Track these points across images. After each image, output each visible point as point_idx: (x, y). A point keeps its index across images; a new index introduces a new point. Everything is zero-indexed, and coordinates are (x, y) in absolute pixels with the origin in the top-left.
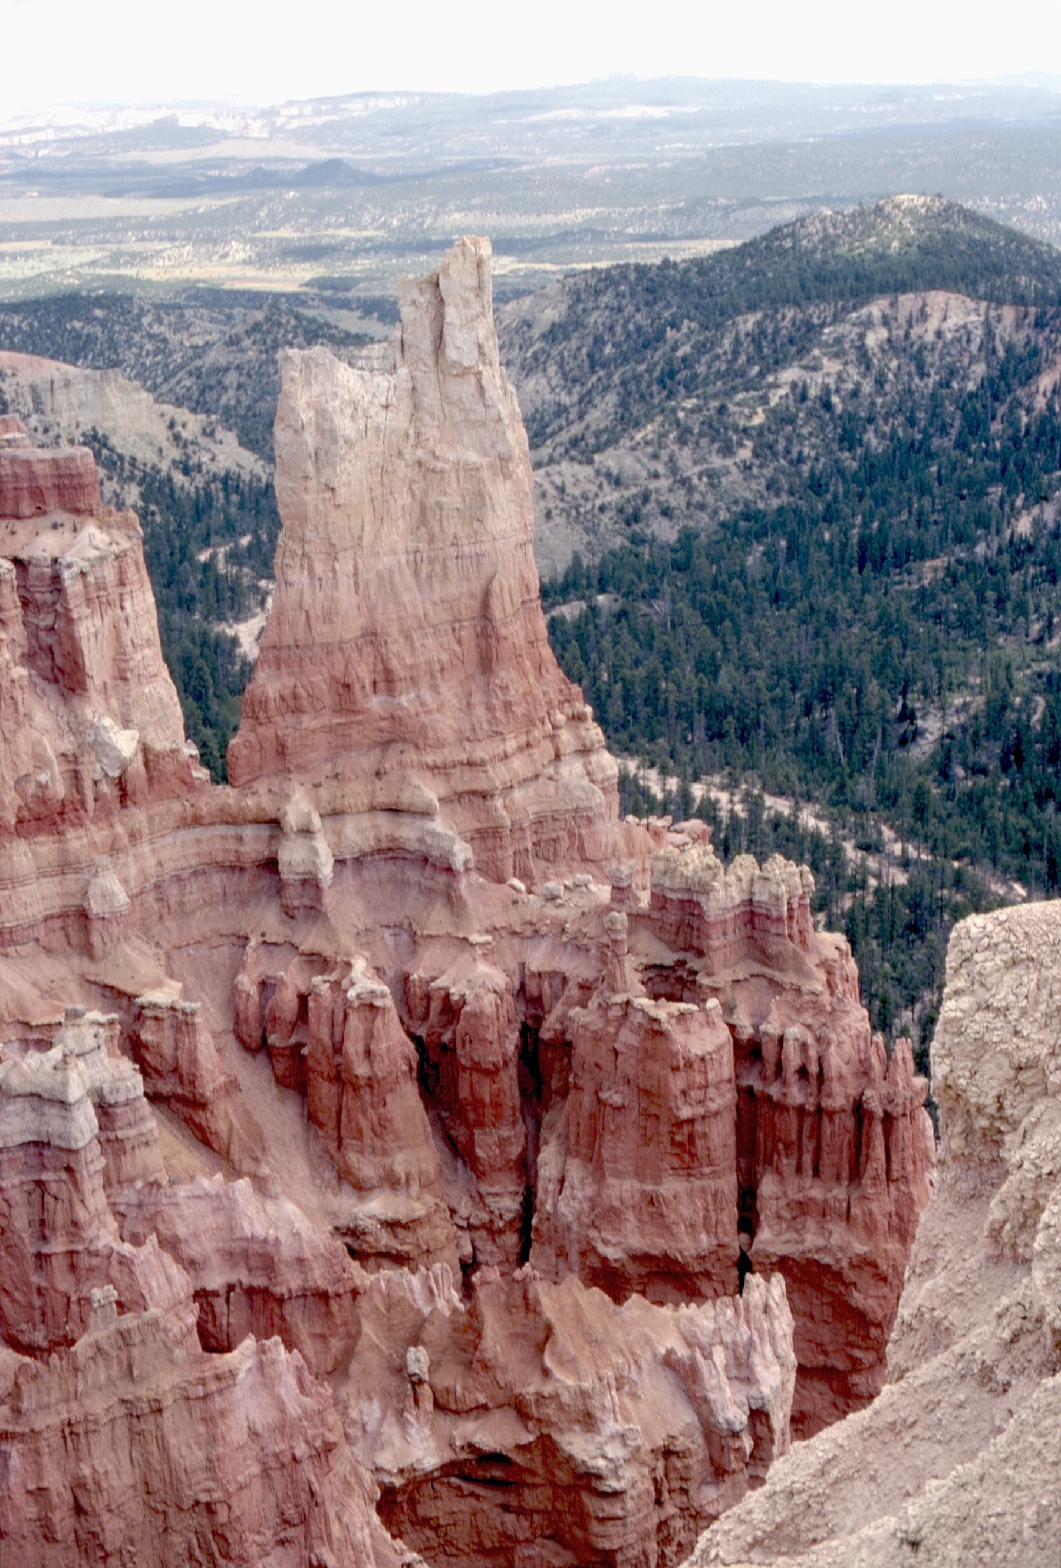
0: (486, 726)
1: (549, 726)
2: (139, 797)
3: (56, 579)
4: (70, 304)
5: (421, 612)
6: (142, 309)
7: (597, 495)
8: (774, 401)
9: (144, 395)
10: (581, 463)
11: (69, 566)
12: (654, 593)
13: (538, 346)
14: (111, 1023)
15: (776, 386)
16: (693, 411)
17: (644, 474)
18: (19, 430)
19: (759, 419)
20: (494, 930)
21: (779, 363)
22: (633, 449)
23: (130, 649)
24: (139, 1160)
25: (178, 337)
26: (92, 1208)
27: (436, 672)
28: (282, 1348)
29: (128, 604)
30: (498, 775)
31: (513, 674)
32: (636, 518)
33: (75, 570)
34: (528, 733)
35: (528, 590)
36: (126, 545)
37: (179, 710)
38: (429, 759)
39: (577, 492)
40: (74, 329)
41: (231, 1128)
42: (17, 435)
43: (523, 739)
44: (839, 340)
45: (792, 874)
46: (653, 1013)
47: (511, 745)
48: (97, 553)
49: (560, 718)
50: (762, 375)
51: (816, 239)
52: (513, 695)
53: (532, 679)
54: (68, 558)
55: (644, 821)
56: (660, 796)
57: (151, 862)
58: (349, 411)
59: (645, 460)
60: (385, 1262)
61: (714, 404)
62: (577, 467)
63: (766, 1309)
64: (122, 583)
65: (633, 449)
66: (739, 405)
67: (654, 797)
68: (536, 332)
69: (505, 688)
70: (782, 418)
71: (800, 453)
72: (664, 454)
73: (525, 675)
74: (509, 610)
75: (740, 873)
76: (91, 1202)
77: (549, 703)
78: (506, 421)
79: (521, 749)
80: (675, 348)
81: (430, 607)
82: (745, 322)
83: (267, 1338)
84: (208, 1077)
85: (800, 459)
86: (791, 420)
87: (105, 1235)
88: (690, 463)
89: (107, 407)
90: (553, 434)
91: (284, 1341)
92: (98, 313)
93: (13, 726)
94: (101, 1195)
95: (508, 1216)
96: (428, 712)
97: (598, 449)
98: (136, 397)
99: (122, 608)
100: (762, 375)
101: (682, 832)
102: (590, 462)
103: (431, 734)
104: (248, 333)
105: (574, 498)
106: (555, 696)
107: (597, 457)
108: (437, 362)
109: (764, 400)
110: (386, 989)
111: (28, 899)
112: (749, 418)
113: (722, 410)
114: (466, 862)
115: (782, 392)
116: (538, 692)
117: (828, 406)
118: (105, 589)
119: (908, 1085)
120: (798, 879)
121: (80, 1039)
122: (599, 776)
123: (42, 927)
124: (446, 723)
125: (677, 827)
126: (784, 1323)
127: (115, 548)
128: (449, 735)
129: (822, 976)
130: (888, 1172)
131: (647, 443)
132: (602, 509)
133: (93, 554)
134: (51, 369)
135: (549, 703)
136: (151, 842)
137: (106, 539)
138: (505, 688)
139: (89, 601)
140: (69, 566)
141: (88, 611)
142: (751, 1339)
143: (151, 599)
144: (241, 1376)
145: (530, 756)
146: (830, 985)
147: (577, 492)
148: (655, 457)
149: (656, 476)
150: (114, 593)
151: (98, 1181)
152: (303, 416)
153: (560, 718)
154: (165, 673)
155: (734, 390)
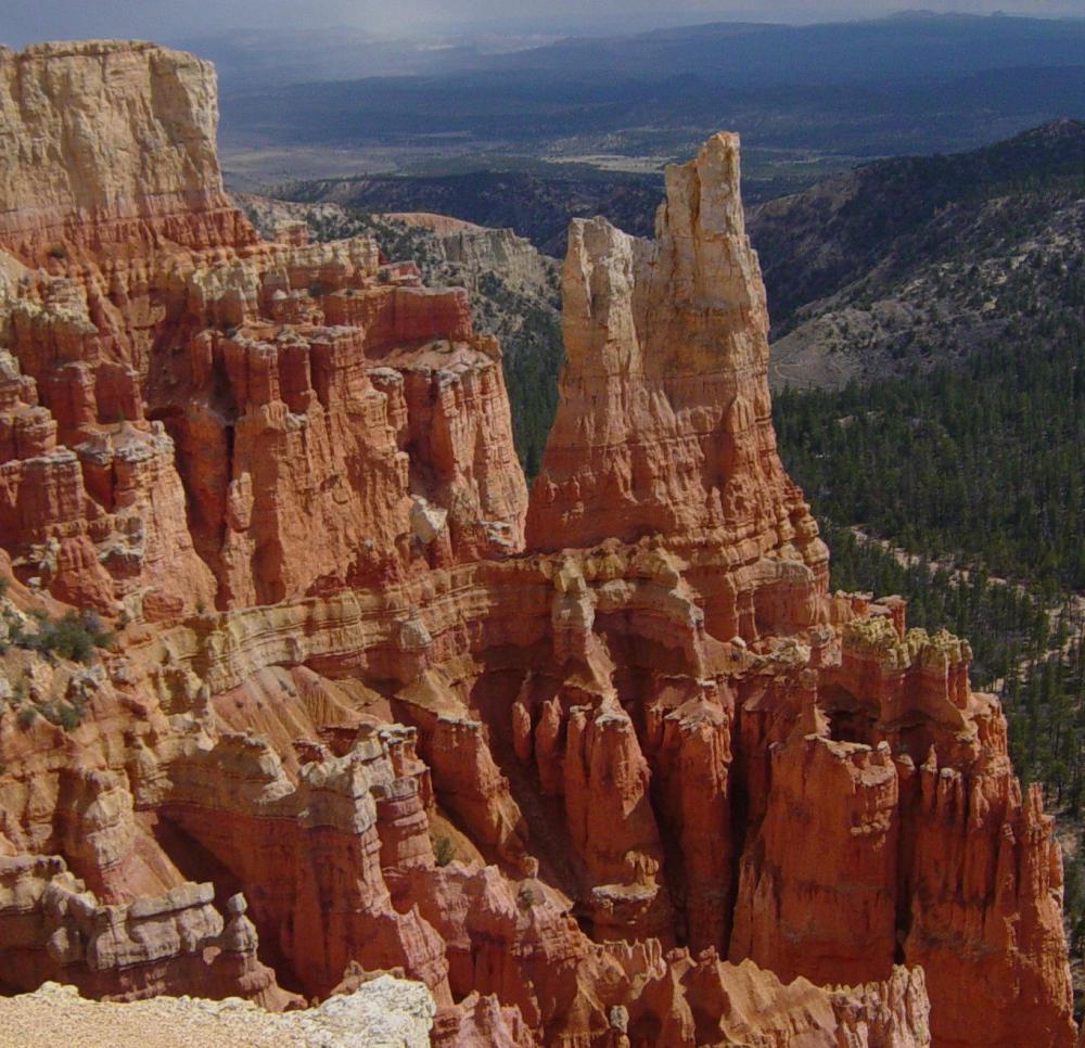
0: (721, 516)
1: (774, 518)
2: (445, 561)
3: (434, 387)
4: (482, 178)
5: (674, 426)
6: (535, 184)
7: (872, 335)
8: (1015, 265)
10: (861, 309)
11: (444, 377)
12: (910, 413)
13: (834, 218)
14: (410, 734)
15: (1017, 254)
16: (951, 272)
17: (910, 319)
18: (415, 273)
19: (1003, 280)
20: (718, 678)
22: (902, 300)
23: (489, 441)
24: (411, 845)
25: (561, 207)
26: (369, 880)
27: (685, 471)
28: (497, 1003)
29: (489, 408)
30: (730, 554)
31: (746, 477)
32: (901, 354)
33: (449, 380)
34: (756, 524)
35: (763, 413)
36: (488, 362)
37: (525, 490)
38: (676, 540)
39: (856, 332)
40: (483, 198)
41: (500, 818)
42: (412, 277)
43: (752, 528)
44: (1068, 220)
45: (955, 646)
46: (834, 751)
47: (742, 532)
48: (466, 368)
49: (784, 512)
50: (1006, 246)
51: (1055, 141)
52: (744, 493)
53: (761, 481)
54: (444, 371)
55: (851, 595)
56: (905, 566)
57: (452, 610)
58: (621, 267)
59: (911, 308)
60: (969, 820)
61: (968, 267)
62: (858, 313)
64: (483, 392)
65: (902, 300)
66: (987, 267)
67: (901, 567)
68: (834, 208)
69: (738, 488)
70: (1019, 279)
71: (1034, 306)
72: (927, 305)
73: (756, 478)
74: (744, 425)
75: (912, 642)
76: (368, 876)
77: (775, 501)
78: (748, 278)
79: (750, 535)
80: (939, 224)
81: (680, 423)
82: (996, 203)
83: (489, 994)
84: (484, 779)
85: (1034, 311)
86: (1028, 281)
87: (378, 901)
88: (946, 312)
89: (502, 257)
90: (842, 286)
91: (499, 999)
92: (502, 186)
93: (396, 497)
94: (377, 870)
95: (716, 903)
96: (675, 504)
97: (877, 299)
99: (484, 411)
100: (1006, 246)
101: (883, 604)
102: (868, 309)
103: (677, 521)
104: (614, 204)
105: (854, 336)
106: (781, 496)
107: (874, 306)
108: (693, 231)
109: (1007, 265)
110: (628, 719)
111: (354, 635)
112: (995, 278)
113: (974, 270)
114: (698, 622)
115: (1022, 259)
116: (767, 492)
117: (1057, 271)
118: (471, 395)
119: (1038, 820)
120: (958, 650)
121: (369, 749)
122: (814, 559)
123: (364, 656)
124: (690, 515)
125: (880, 600)
126: (922, 1006)
127: (480, 365)
128: (692, 523)
129: (975, 729)
130: (1017, 889)
131: (913, 295)
132: (876, 346)
133: (463, 368)
134: (456, 227)
135: (775, 501)
136: (453, 595)
137: (474, 357)
138: (738, 488)
139: (458, 405)
140: (444, 377)
141: (457, 412)
142: (890, 1020)
143: (507, 405)
144: (462, 1023)
145: (757, 541)
146: (982, 735)
147: (856, 332)
148: (918, 306)
149: (918, 322)
150: (478, 401)
151: (376, 858)
152: (584, 270)
153: (784, 512)
154: (515, 461)
155: (985, 257)
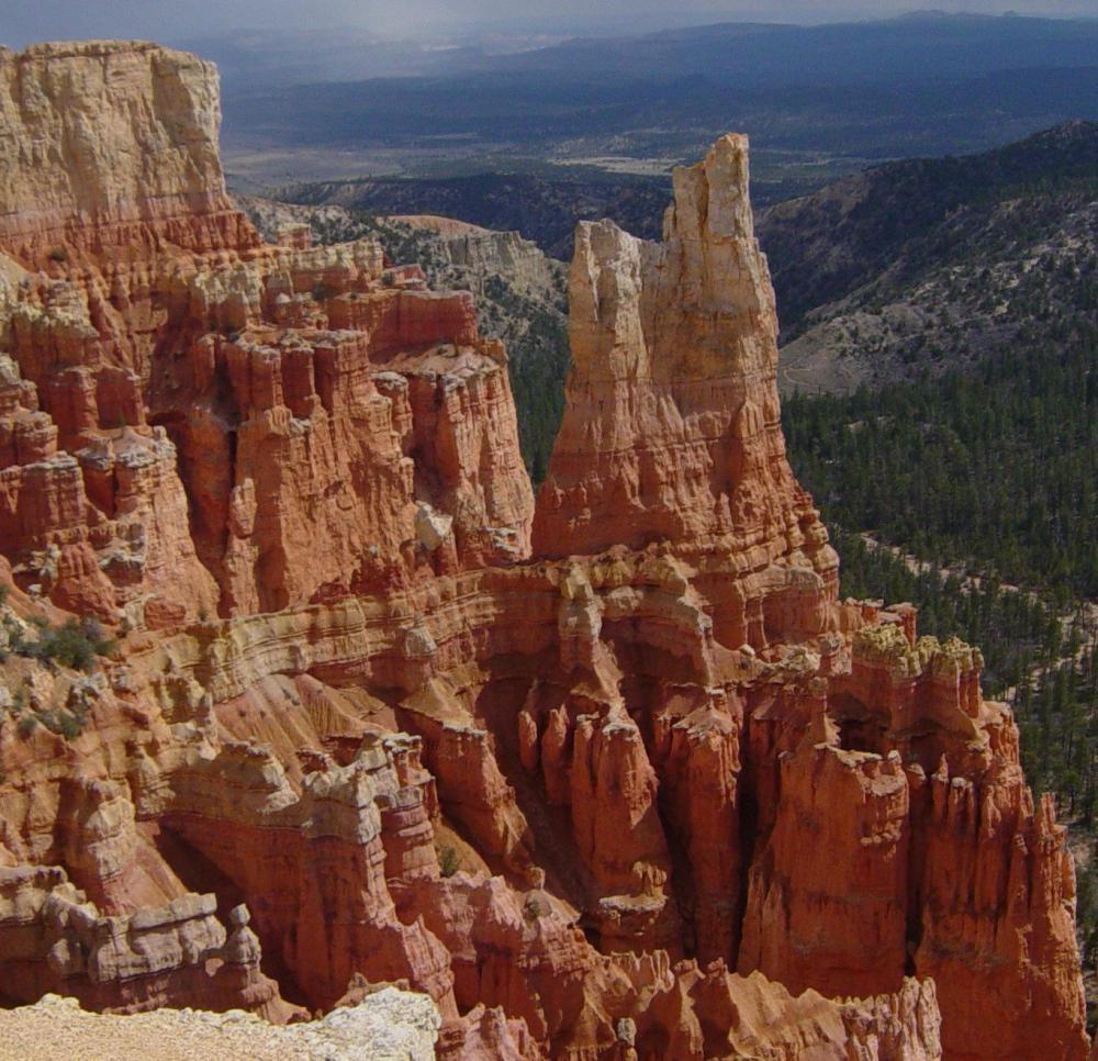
0: (730, 523)
1: (783, 525)
2: (451, 568)
3: (440, 392)
4: (488, 180)
5: (682, 431)
6: (541, 186)
7: (882, 339)
8: (1027, 268)
9: (537, 251)
10: (871, 313)
11: (449, 382)
12: (921, 418)
13: (844, 221)
14: (415, 743)
15: (1029, 257)
16: (962, 275)
17: (920, 323)
18: (419, 277)
19: (1015, 283)
20: (726, 687)
21: (1033, 240)
22: (913, 303)
23: (494, 447)
24: (416, 855)
25: (568, 209)
26: (373, 891)
27: (693, 476)
28: (503, 1015)
29: (495, 413)
30: (739, 561)
31: (755, 483)
33: (454, 385)
34: (765, 530)
35: (772, 418)
36: (494, 367)
37: (531, 496)
38: (684, 546)
39: (866, 336)
40: (489, 200)
41: (506, 828)
42: (417, 280)
43: (761, 534)
44: (1080, 223)
45: (966, 654)
46: (844, 760)
47: (751, 538)
48: (472, 373)
49: (794, 518)
50: (1018, 249)
51: (1068, 143)
52: (753, 499)
53: (770, 487)
54: (450, 376)
55: (861, 603)
56: (916, 573)
57: (458, 617)
58: (629, 270)
59: (922, 312)
60: (981, 830)
61: (979, 270)
62: (869, 317)
63: (917, 1008)
64: (489, 397)
65: (913, 303)
66: (999, 271)
67: (912, 574)
68: (844, 210)
69: (747, 494)
70: (1032, 283)
71: (1046, 310)
72: (938, 309)
73: (765, 484)
74: (753, 431)
75: (923, 650)
76: (372, 887)
77: (785, 507)
78: (757, 281)
79: (759, 542)
80: (950, 227)
81: (689, 428)
82: (1008, 206)
83: (495, 1007)
84: (489, 789)
86: (1040, 285)
87: (382, 912)
88: (957, 316)
89: (508, 261)
90: (853, 290)
91: (505, 1011)
92: (508, 188)
93: (401, 503)
94: (382, 881)
95: (724, 914)
96: (683, 510)
97: (887, 303)
98: (530, 252)
99: (490, 416)
100: (1018, 249)
101: (894, 612)
102: (878, 313)
104: (621, 206)
105: (864, 340)
106: (790, 502)
107: (885, 309)
108: (702, 234)
109: (1019, 269)
110: (635, 727)
111: (358, 643)
112: (1007, 282)
113: (986, 273)
114: (707, 630)
115: (1034, 262)
116: (776, 498)
117: (1070, 275)
118: (477, 400)
119: (1051, 830)
120: (970, 658)
121: (373, 758)
122: (823, 566)
123: (368, 664)
124: (698, 521)
125: (891, 608)
126: (933, 1018)
127: (486, 369)
128: (700, 530)
129: (986, 738)
130: (1029, 900)
131: (924, 299)
132: (886, 350)
133: (469, 373)
134: (461, 230)
135: (785, 507)
136: (459, 602)
137: (479, 362)
138: (747, 494)
139: (463, 410)
140: (449, 382)
141: (463, 417)
142: (901, 1033)
143: (513, 410)
144: (467, 1036)
145: (766, 547)
146: (993, 745)
147: (866, 336)
148: (929, 310)
149: (929, 326)
150: (484, 406)
151: (380, 869)
152: (591, 273)
153: (794, 518)
155: (996, 260)
